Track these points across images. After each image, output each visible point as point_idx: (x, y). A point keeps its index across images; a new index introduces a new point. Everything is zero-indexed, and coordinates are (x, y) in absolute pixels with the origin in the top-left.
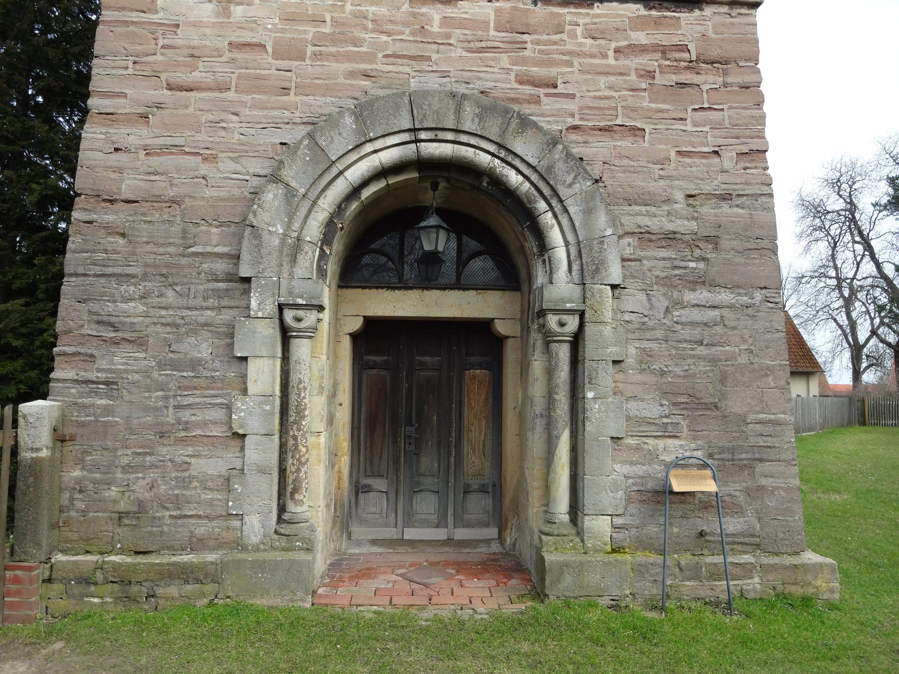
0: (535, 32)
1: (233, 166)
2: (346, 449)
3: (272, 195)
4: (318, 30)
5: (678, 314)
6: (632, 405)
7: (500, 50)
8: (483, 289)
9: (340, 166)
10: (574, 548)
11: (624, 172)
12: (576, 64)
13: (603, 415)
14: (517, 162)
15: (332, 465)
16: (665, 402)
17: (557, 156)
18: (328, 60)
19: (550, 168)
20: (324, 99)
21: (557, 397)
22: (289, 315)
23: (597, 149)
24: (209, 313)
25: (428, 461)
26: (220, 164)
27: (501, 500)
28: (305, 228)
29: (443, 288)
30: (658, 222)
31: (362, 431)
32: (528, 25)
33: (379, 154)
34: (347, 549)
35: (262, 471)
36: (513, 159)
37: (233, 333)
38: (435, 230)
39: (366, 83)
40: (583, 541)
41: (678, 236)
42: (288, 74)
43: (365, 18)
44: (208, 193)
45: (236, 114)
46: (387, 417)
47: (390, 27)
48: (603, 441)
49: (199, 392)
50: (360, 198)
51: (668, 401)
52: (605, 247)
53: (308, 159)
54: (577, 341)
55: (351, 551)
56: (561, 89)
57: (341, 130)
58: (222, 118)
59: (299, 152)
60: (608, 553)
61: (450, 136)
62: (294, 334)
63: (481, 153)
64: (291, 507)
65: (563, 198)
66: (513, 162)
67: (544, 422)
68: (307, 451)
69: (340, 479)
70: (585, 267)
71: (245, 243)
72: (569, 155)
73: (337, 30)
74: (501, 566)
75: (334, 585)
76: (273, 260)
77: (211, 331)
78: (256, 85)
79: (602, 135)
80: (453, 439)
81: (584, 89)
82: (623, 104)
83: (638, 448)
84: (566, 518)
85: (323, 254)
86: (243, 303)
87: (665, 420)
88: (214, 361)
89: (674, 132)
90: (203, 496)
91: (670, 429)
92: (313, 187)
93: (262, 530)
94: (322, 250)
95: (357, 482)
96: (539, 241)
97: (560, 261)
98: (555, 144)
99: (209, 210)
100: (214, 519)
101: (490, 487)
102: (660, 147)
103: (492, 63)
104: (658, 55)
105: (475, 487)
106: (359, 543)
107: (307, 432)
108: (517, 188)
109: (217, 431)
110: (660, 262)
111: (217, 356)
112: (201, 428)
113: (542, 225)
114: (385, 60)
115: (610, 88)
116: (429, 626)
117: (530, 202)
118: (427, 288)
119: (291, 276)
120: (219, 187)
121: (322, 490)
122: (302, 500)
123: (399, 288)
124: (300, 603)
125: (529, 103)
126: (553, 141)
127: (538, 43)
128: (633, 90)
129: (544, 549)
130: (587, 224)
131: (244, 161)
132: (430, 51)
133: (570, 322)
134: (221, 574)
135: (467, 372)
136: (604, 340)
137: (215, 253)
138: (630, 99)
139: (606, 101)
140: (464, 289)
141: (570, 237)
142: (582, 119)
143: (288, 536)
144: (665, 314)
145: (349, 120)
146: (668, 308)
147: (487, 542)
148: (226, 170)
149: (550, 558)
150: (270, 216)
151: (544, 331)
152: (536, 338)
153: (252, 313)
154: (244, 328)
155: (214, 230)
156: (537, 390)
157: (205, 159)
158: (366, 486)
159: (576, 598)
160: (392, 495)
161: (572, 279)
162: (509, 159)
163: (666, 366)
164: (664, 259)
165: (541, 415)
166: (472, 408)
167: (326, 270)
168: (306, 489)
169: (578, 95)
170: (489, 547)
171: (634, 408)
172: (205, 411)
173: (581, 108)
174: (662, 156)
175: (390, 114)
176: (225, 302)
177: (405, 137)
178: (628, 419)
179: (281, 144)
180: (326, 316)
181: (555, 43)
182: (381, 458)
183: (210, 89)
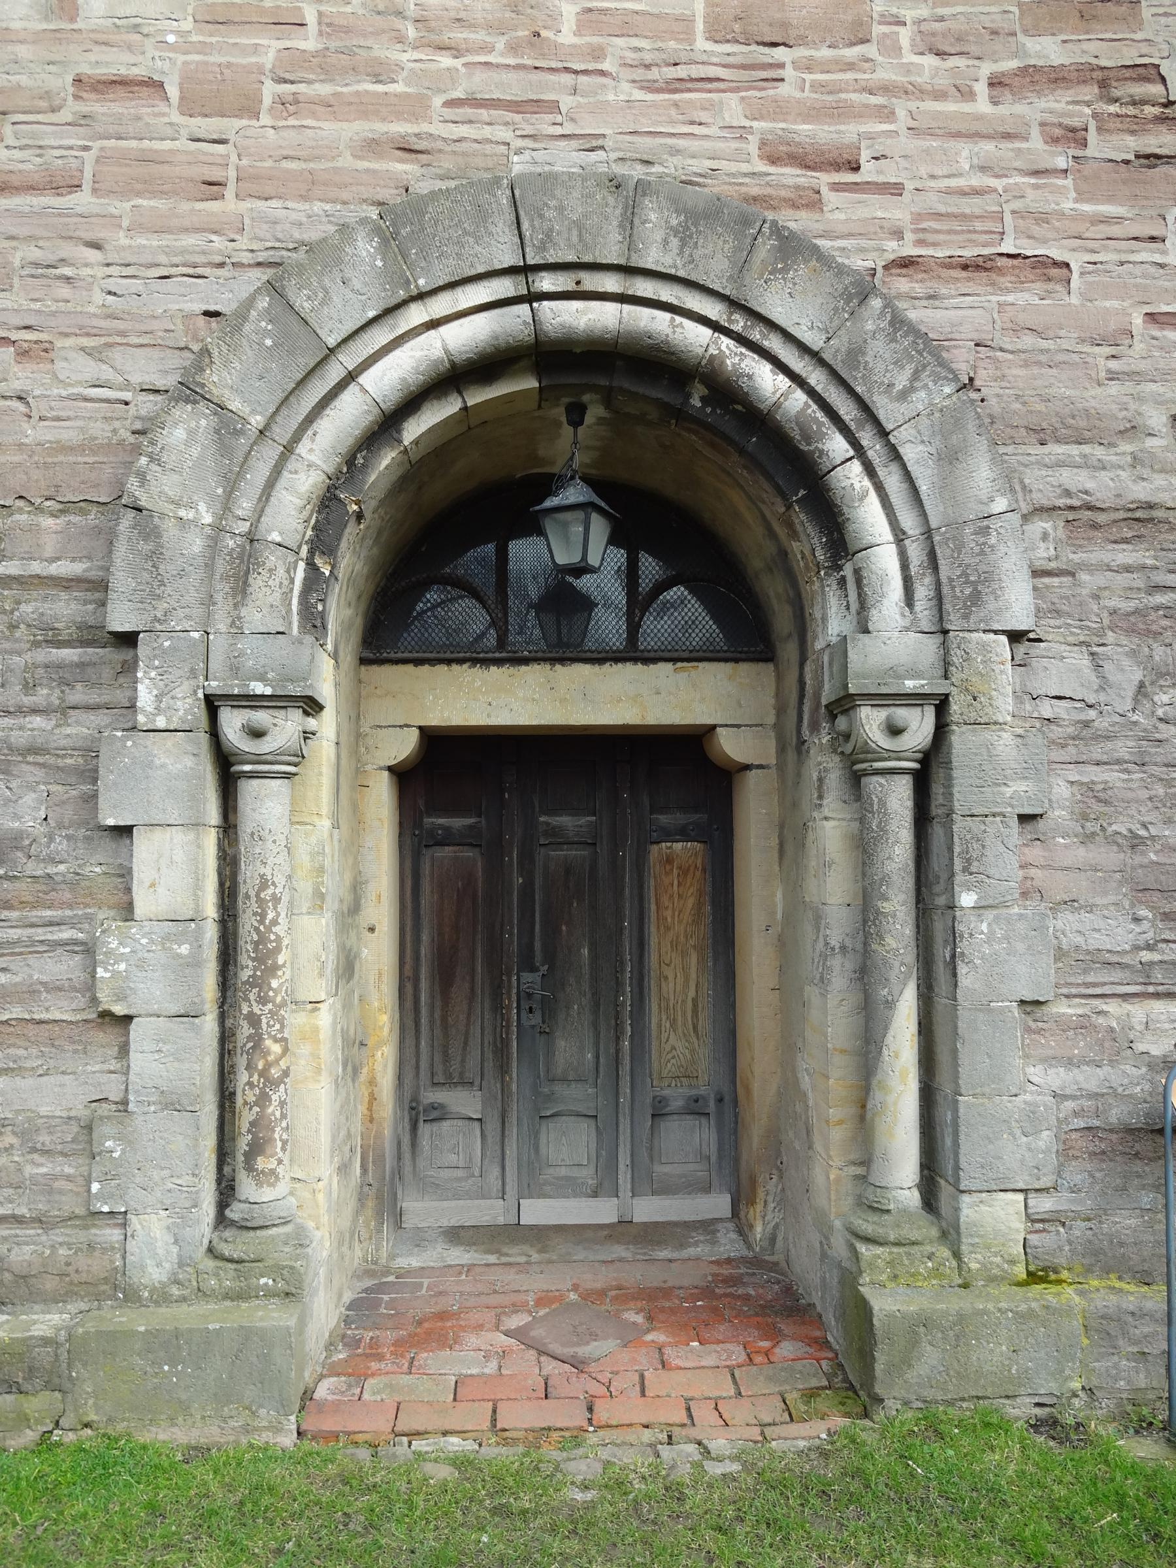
0: (802, 41)
1: (90, 369)
2: (386, 1030)
3: (184, 432)
4: (288, 44)
5: (1165, 698)
6: (1067, 921)
7: (721, 85)
8: (688, 660)
9: (348, 360)
10: (936, 1273)
11: (1026, 364)
12: (901, 113)
13: (998, 950)
14: (774, 344)
15: (353, 1066)
16: (1143, 912)
17: (870, 326)
18: (314, 115)
19: (855, 354)
20: (307, 206)
21: (886, 907)
22: (232, 723)
23: (959, 314)
24: (38, 721)
25: (571, 1048)
26: (59, 364)
27: (736, 1131)
28: (268, 510)
29: (600, 658)
30: (1110, 482)
31: (424, 985)
32: (785, 25)
33: (443, 330)
34: (392, 1257)
35: (172, 1103)
36: (764, 337)
37: (96, 770)
38: (580, 515)
39: (407, 167)
40: (957, 1255)
41: (1159, 514)
42: (220, 148)
43: (399, 14)
44: (32, 433)
45: (96, 246)
46: (479, 953)
47: (459, 35)
48: (1001, 1011)
49: (15, 914)
50: (400, 442)
51: (1152, 908)
52: (993, 541)
53: (269, 342)
54: (928, 772)
55: (402, 1262)
56: (869, 171)
57: (349, 273)
58: (63, 254)
59: (247, 328)
60: (1019, 1284)
61: (611, 283)
62: (247, 768)
63: (689, 324)
64: (247, 1188)
65: (889, 426)
66: (766, 343)
67: (849, 965)
68: (286, 1050)
69: (373, 1098)
70: (945, 590)
71: (121, 550)
72: (898, 323)
73: (333, 45)
74: (746, 1298)
75: (357, 1375)
76: (190, 590)
77: (43, 765)
78: (145, 175)
79: (969, 279)
80: (626, 999)
81: (923, 171)
82: (1017, 205)
83: (1083, 1025)
84: (912, 1198)
85: (313, 576)
86: (121, 697)
87: (1146, 956)
88: (51, 839)
89: (1138, 270)
90: (29, 1170)
91: (1158, 976)
92: (284, 411)
93: (175, 1249)
94: (311, 565)
95: (415, 1099)
96: (829, 535)
97: (884, 578)
98: (864, 299)
99: (36, 474)
100: (54, 1226)
101: (712, 1103)
102: (1108, 304)
103: (703, 116)
104: (1090, 92)
105: (677, 1104)
106: (419, 1240)
107: (284, 1004)
108: (777, 405)
109: (62, 1009)
110: (1119, 577)
111: (60, 826)
112: (21, 1002)
113: (839, 493)
114: (449, 113)
115: (983, 169)
116: (590, 1506)
117: (808, 439)
118: (562, 661)
119: (237, 628)
120: (58, 419)
121: (324, 1139)
122: (272, 1172)
123: (499, 662)
124: (267, 1436)
125: (795, 206)
126: (861, 290)
127: (809, 66)
128: (1036, 173)
129: (866, 1278)
130: (947, 485)
131: (116, 355)
132: (555, 88)
133: (914, 725)
134: (70, 1366)
135: (654, 849)
136: (997, 765)
137: (51, 578)
138: (1031, 194)
139: (977, 200)
140: (647, 660)
141: (909, 521)
142: (920, 243)
143: (240, 1261)
144: (1136, 700)
145: (365, 248)
146: (1141, 685)
147: (707, 1227)
148: (74, 377)
149: (885, 1303)
150: (181, 482)
151: (848, 748)
152: (823, 763)
153: (141, 719)
154: (122, 757)
155: (48, 522)
156: (833, 889)
157: (23, 354)
158: (433, 1107)
159: (950, 1403)
160: (493, 1126)
161: (915, 621)
162: (756, 335)
163: (1144, 826)
164: (1128, 569)
165: (843, 948)
166: (668, 929)
167: (323, 615)
168: (285, 1143)
169: (909, 186)
170: (714, 1242)
171: (1071, 927)
172: (32, 959)
173: (918, 217)
174: (1112, 326)
175: (466, 233)
176: (78, 695)
177: (504, 287)
178: (1060, 954)
179: (208, 314)
180: (327, 725)
181: (851, 66)
182: (466, 1043)
183: (32, 188)
